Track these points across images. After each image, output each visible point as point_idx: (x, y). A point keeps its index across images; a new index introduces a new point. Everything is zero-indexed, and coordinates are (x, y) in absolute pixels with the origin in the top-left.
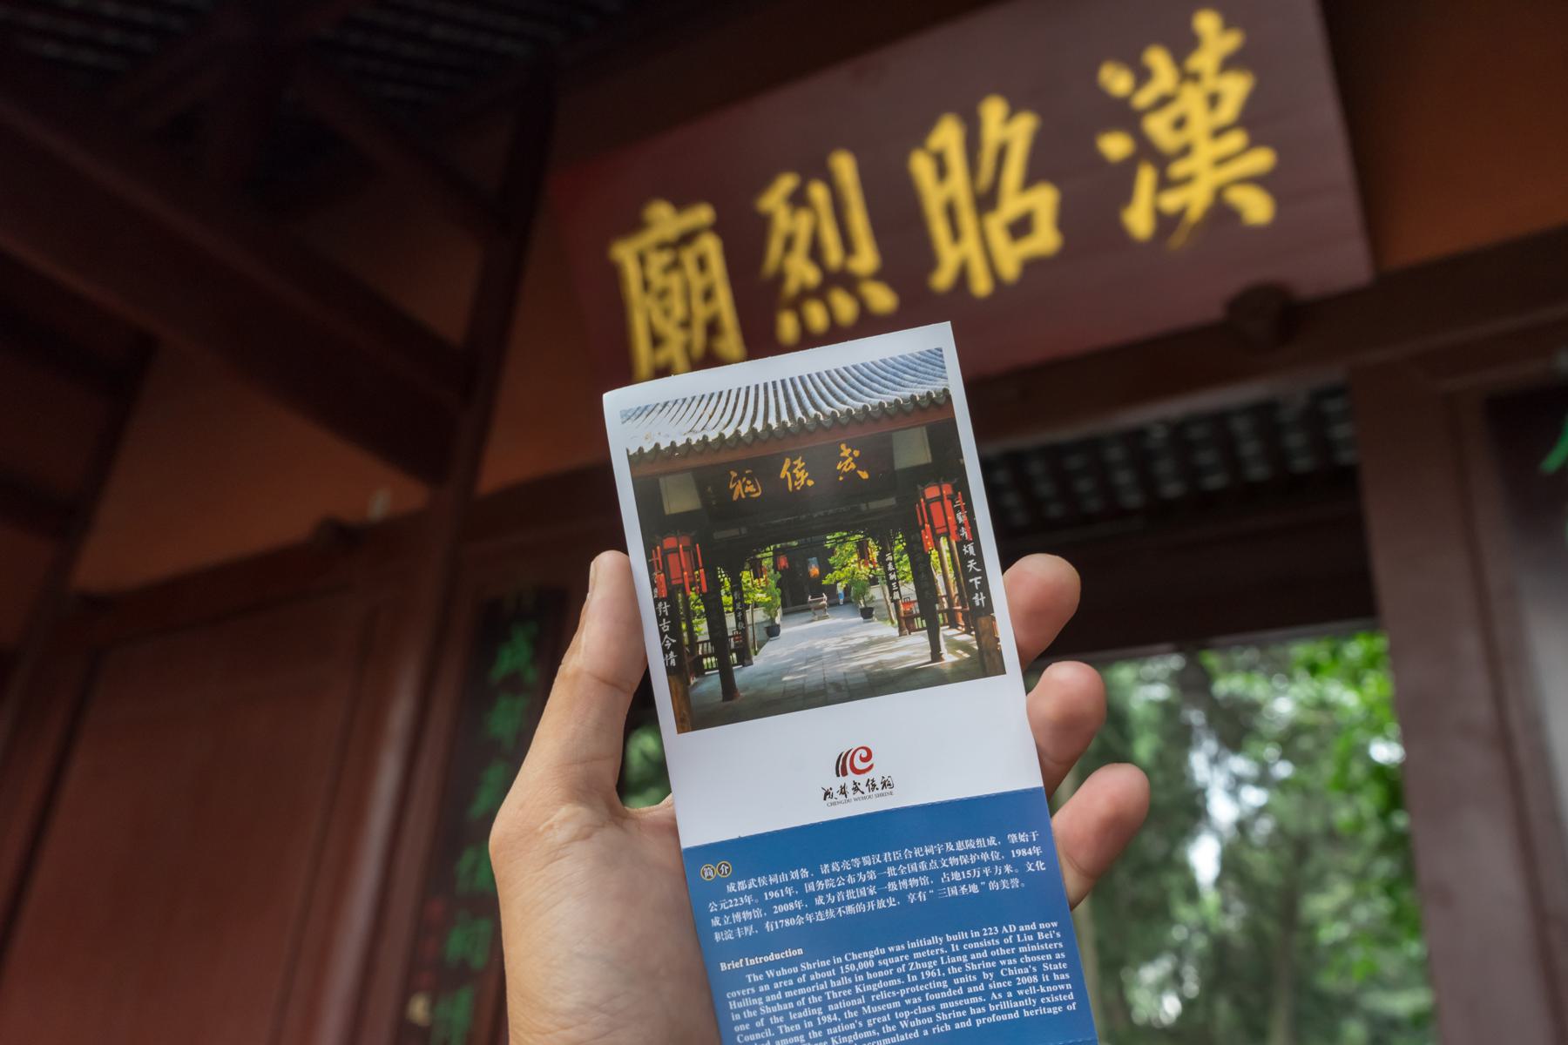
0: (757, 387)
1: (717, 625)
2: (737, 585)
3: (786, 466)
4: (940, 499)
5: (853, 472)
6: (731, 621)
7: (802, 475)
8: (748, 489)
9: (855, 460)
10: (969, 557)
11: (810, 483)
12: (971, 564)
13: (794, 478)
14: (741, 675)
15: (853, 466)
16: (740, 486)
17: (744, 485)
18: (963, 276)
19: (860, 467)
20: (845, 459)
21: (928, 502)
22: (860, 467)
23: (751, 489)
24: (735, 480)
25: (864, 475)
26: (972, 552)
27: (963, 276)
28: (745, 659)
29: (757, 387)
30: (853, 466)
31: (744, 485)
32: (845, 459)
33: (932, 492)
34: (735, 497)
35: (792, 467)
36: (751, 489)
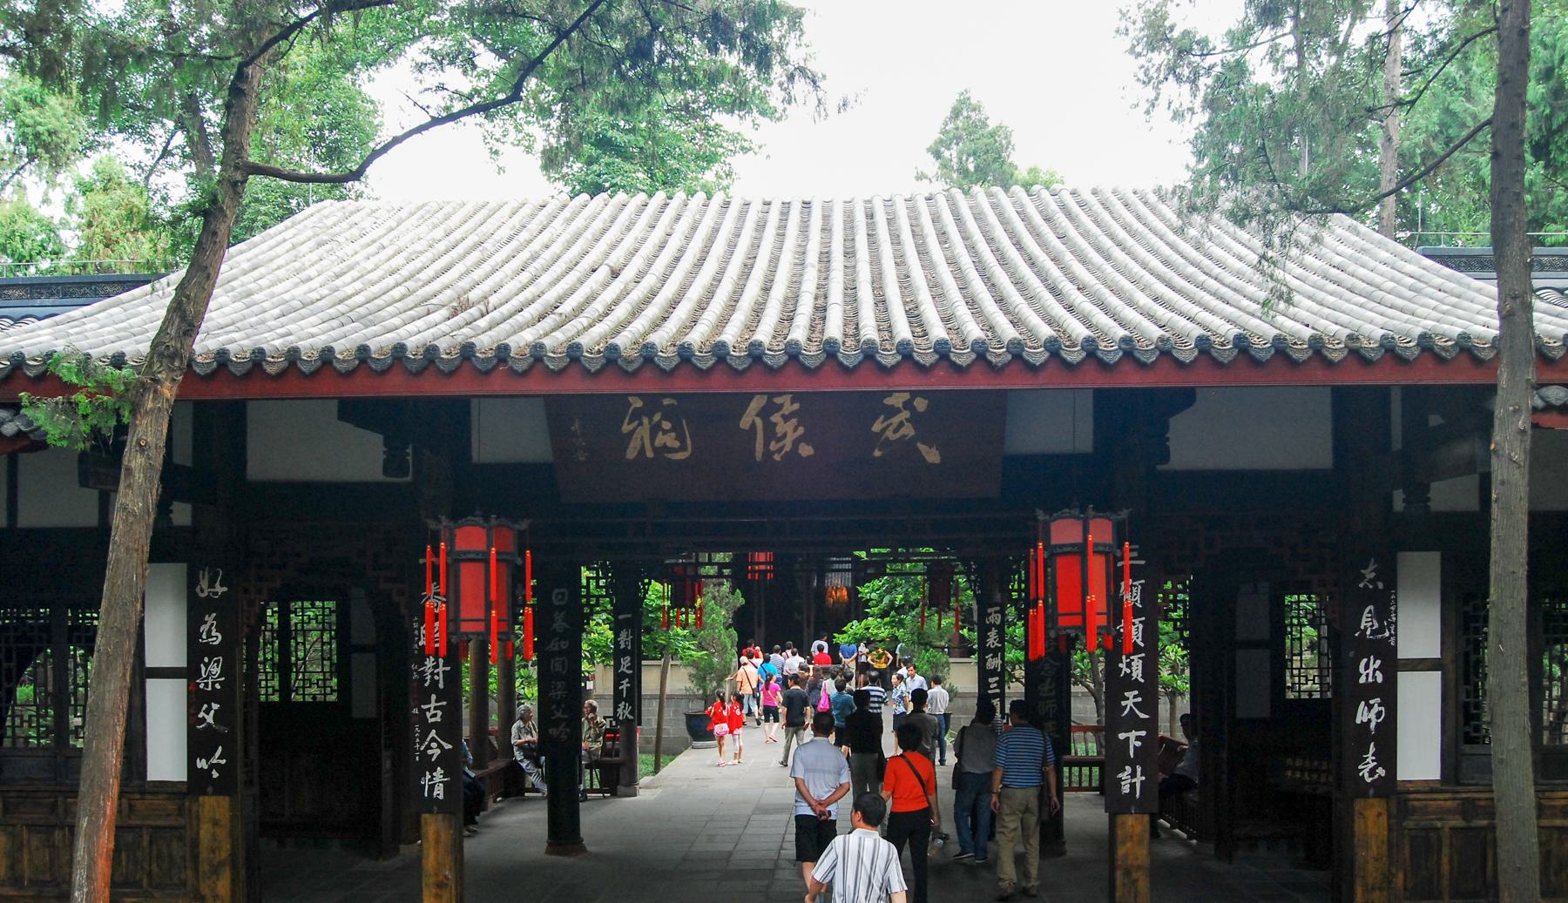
0: (786, 206)
1: (563, 693)
2: (629, 614)
3: (756, 404)
4: (1081, 551)
5: (907, 445)
6: (599, 680)
7: (789, 431)
8: (661, 439)
9: (916, 419)
10: (1130, 683)
11: (806, 450)
12: (1131, 699)
13: (770, 429)
14: (600, 817)
15: (909, 431)
16: (644, 431)
17: (655, 429)
18: (642, 450)
19: (925, 435)
20: (893, 411)
21: (1054, 553)
22: (925, 435)
23: (670, 440)
24: (637, 415)
25: (932, 456)
26: (1137, 672)
27: (642, 450)
28: (618, 778)
29: (786, 206)
30: (909, 431)
31: (655, 429)
32: (893, 411)
33: (1065, 531)
34: (631, 454)
35: (765, 413)
36: (670, 440)
